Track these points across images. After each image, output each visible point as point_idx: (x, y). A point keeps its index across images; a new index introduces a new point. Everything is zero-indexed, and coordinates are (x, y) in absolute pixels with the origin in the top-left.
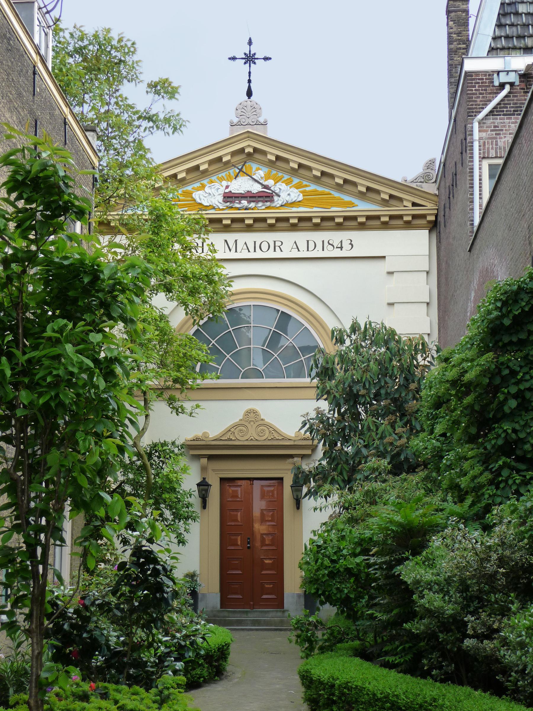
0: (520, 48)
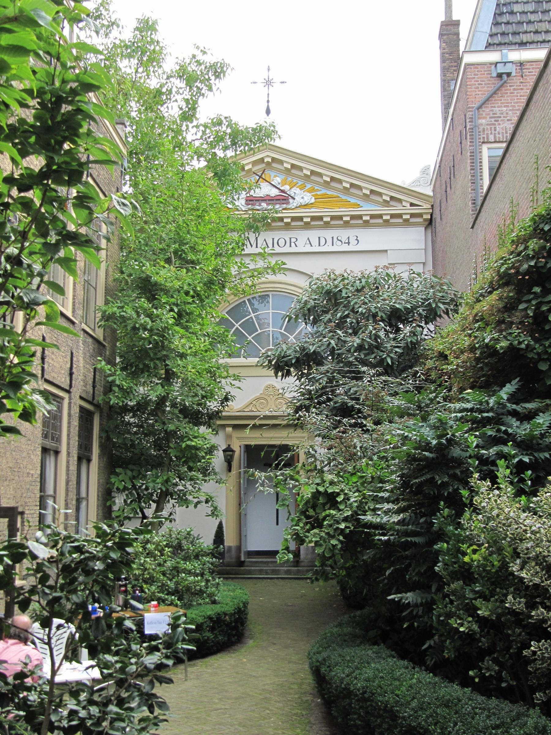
0: (516, 44)
